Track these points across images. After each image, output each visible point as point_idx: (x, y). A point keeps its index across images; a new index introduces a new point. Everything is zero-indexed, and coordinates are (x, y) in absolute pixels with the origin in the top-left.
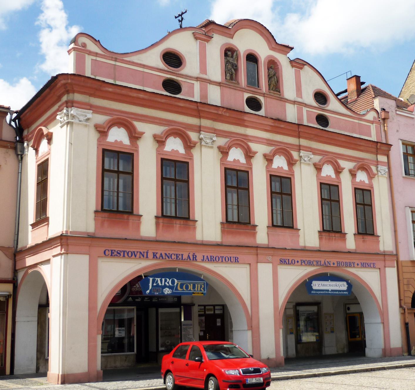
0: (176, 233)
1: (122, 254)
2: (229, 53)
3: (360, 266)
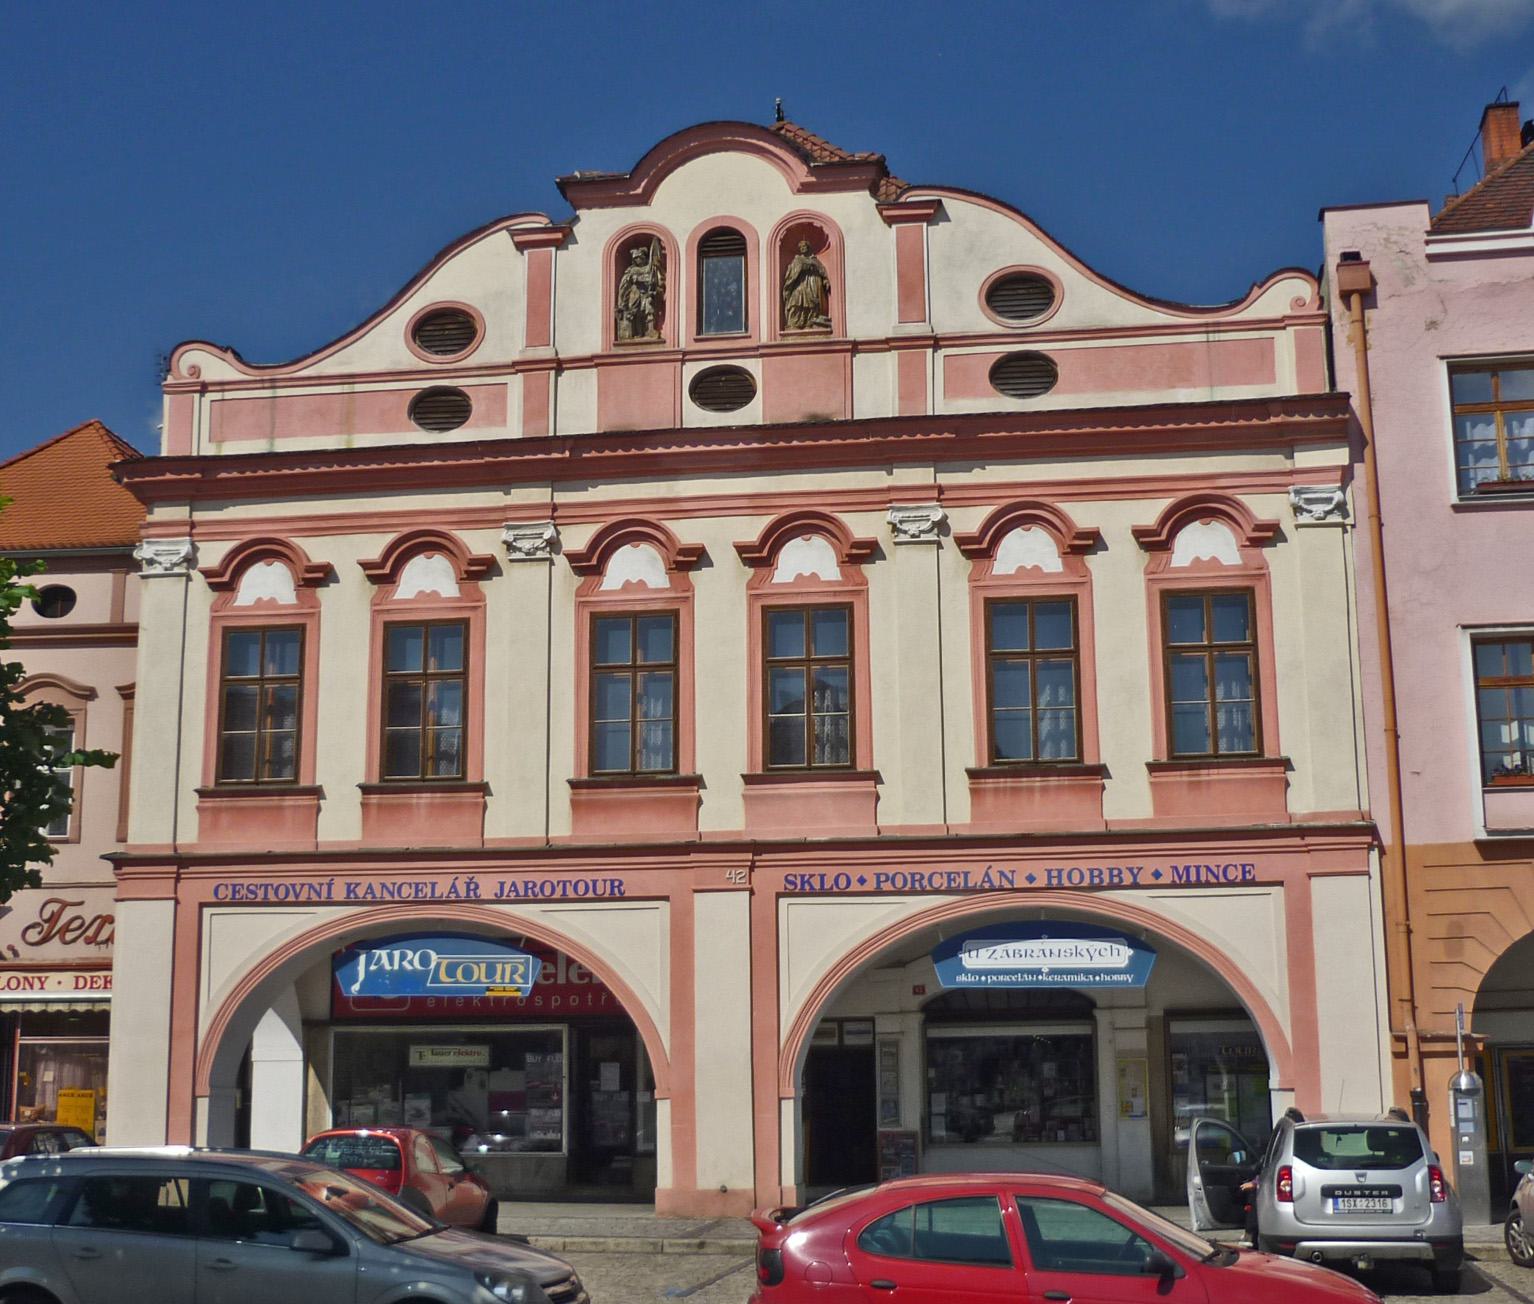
0: (422, 823)
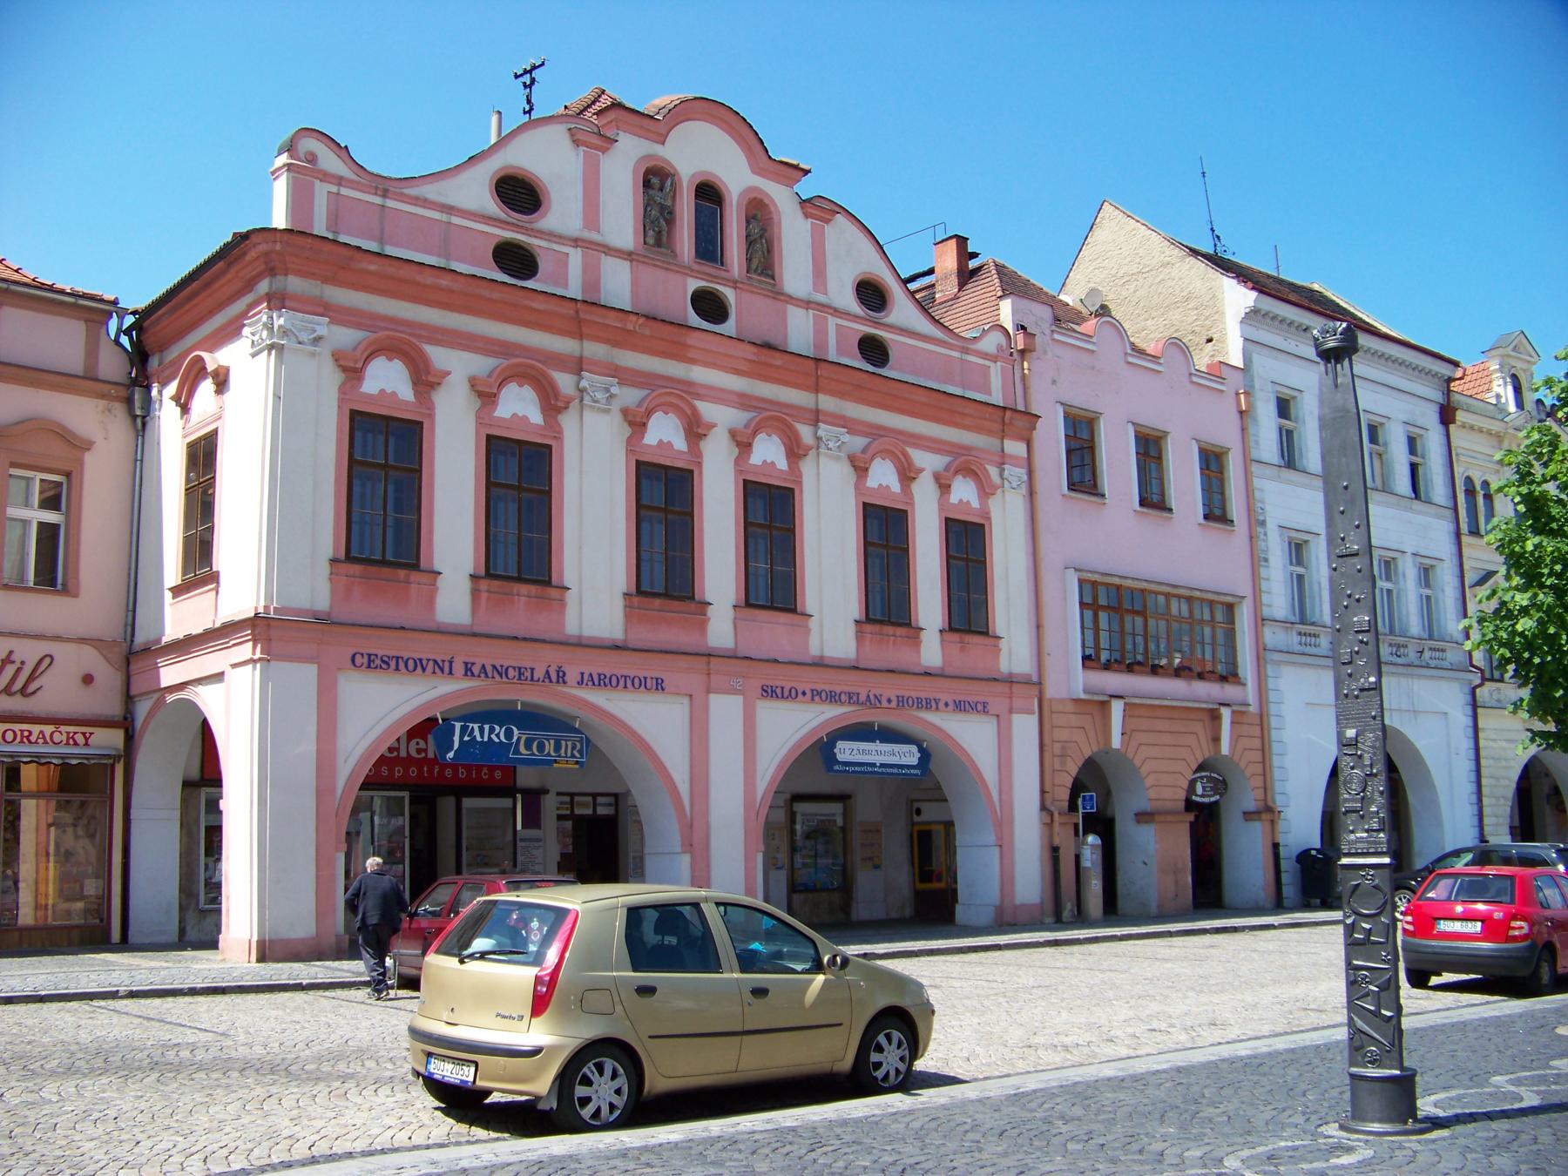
0: (520, 610)
2: (655, 179)
3: (951, 705)
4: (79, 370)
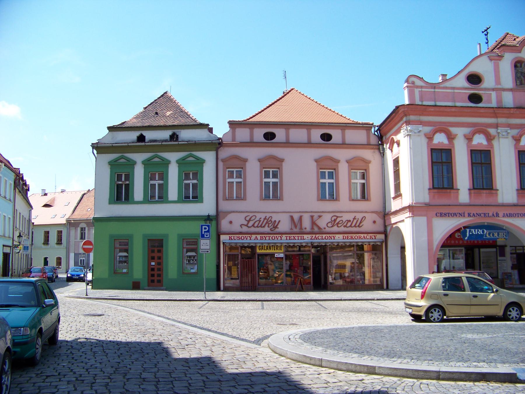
0: (484, 198)
1: (447, 215)
4: (366, 143)
